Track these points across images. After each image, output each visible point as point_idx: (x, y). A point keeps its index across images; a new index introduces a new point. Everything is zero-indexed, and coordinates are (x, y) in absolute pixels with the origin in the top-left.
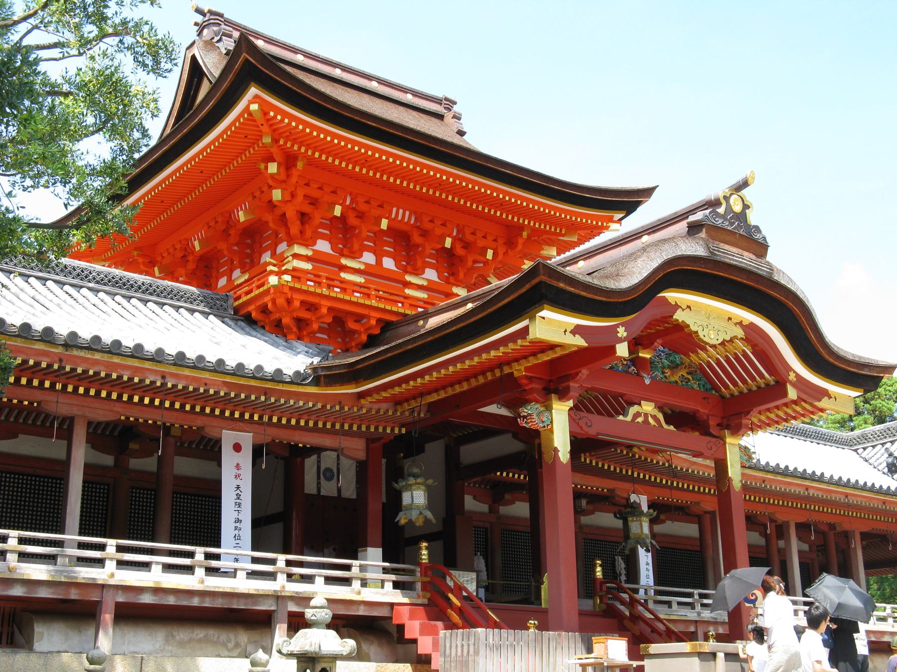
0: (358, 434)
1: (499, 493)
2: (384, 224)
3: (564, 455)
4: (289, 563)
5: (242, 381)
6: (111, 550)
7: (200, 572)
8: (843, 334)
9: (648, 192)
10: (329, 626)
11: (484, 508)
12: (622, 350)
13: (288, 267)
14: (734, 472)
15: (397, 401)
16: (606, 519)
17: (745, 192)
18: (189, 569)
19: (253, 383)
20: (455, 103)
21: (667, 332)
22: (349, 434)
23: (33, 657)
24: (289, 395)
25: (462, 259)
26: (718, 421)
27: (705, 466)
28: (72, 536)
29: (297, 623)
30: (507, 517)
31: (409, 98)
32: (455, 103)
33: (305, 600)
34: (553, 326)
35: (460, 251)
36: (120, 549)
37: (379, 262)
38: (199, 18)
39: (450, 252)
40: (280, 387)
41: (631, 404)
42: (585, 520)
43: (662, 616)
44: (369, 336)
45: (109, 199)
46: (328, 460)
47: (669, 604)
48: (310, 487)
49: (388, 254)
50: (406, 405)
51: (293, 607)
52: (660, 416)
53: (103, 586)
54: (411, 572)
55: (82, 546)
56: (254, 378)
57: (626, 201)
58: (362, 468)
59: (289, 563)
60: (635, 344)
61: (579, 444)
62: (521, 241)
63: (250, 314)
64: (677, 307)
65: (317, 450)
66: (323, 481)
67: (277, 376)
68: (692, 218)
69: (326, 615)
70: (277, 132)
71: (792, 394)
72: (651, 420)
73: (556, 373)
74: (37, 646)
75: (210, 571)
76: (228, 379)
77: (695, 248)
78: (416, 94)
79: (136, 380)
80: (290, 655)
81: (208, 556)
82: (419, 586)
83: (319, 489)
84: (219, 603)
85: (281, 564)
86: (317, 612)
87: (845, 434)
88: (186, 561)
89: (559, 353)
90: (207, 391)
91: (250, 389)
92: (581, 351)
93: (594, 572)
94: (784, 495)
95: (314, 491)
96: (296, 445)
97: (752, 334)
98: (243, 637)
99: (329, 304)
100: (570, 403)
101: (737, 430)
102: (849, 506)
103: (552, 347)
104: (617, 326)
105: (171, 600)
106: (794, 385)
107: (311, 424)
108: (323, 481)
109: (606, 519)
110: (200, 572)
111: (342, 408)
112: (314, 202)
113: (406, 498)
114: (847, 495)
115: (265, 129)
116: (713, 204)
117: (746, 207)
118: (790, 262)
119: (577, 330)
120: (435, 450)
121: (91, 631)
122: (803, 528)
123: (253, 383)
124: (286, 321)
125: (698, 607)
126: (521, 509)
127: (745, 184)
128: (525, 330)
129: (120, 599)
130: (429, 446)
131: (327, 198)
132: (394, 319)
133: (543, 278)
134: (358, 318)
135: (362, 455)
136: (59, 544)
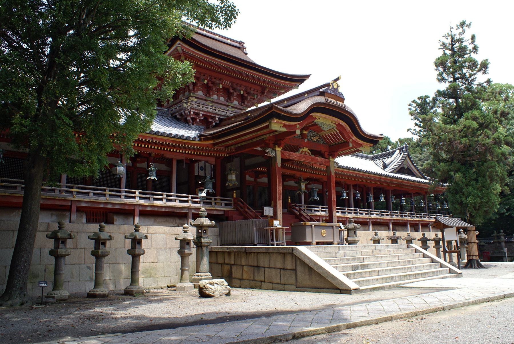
0: (213, 156)
1: (257, 175)
2: (221, 87)
3: (279, 165)
4: (192, 198)
5: (177, 140)
6: (165, 196)
7: (165, 201)
8: (368, 127)
9: (308, 76)
10: (206, 217)
11: (252, 179)
12: (298, 132)
13: (192, 105)
14: (332, 169)
15: (226, 147)
16: (292, 183)
17: (338, 82)
19: (181, 140)
21: (313, 125)
22: (211, 156)
23: (115, 226)
24: (192, 144)
25: (246, 98)
26: (328, 153)
27: (324, 168)
28: (123, 189)
29: (196, 216)
30: (260, 183)
33: (199, 209)
34: (277, 126)
35: (246, 95)
37: (218, 99)
39: (243, 95)
40: (189, 142)
41: (301, 148)
42: (285, 183)
43: (309, 214)
44: (216, 123)
45: (157, 99)
46: (202, 164)
47: (311, 210)
48: (196, 174)
50: (230, 148)
51: (193, 211)
52: (310, 152)
54: (230, 201)
55: (126, 192)
56: (181, 139)
57: (300, 79)
58: (214, 169)
60: (301, 131)
61: (283, 160)
62: (266, 92)
63: (176, 116)
64: (316, 118)
65: (198, 161)
66: (200, 171)
67: (188, 138)
68: (321, 90)
69: (206, 213)
71: (351, 145)
73: (278, 139)
74: (115, 223)
75: (168, 200)
76: (173, 139)
77: (321, 99)
78: (231, 40)
79: (144, 140)
80: (195, 226)
81: (167, 195)
82: (233, 205)
83: (198, 174)
84: (171, 210)
87: (371, 156)
88: (104, 192)
89: (276, 133)
90: (166, 143)
91: (180, 142)
92: (285, 133)
93: (288, 200)
94: (349, 176)
95: (197, 174)
96: (192, 160)
97: (339, 125)
98: (178, 221)
100: (282, 148)
101: (334, 157)
102: (369, 180)
103: (276, 131)
104: (297, 124)
105: (156, 209)
106: (351, 142)
107: (198, 153)
108: (200, 171)
109: (292, 183)
110: (165, 201)
111: (209, 148)
113: (229, 177)
114: (369, 176)
115: (182, 55)
116: (327, 85)
117: (338, 87)
118: (352, 104)
119: (284, 126)
120: (237, 160)
121: (132, 219)
122: (355, 187)
123: (181, 140)
124: (189, 118)
125: (320, 211)
126: (265, 180)
127: (338, 79)
128: (267, 127)
129: (141, 209)
130: (235, 160)
131: (202, 77)
132: (223, 118)
133: (274, 110)
134: (213, 118)
135: (214, 163)
136: (120, 191)
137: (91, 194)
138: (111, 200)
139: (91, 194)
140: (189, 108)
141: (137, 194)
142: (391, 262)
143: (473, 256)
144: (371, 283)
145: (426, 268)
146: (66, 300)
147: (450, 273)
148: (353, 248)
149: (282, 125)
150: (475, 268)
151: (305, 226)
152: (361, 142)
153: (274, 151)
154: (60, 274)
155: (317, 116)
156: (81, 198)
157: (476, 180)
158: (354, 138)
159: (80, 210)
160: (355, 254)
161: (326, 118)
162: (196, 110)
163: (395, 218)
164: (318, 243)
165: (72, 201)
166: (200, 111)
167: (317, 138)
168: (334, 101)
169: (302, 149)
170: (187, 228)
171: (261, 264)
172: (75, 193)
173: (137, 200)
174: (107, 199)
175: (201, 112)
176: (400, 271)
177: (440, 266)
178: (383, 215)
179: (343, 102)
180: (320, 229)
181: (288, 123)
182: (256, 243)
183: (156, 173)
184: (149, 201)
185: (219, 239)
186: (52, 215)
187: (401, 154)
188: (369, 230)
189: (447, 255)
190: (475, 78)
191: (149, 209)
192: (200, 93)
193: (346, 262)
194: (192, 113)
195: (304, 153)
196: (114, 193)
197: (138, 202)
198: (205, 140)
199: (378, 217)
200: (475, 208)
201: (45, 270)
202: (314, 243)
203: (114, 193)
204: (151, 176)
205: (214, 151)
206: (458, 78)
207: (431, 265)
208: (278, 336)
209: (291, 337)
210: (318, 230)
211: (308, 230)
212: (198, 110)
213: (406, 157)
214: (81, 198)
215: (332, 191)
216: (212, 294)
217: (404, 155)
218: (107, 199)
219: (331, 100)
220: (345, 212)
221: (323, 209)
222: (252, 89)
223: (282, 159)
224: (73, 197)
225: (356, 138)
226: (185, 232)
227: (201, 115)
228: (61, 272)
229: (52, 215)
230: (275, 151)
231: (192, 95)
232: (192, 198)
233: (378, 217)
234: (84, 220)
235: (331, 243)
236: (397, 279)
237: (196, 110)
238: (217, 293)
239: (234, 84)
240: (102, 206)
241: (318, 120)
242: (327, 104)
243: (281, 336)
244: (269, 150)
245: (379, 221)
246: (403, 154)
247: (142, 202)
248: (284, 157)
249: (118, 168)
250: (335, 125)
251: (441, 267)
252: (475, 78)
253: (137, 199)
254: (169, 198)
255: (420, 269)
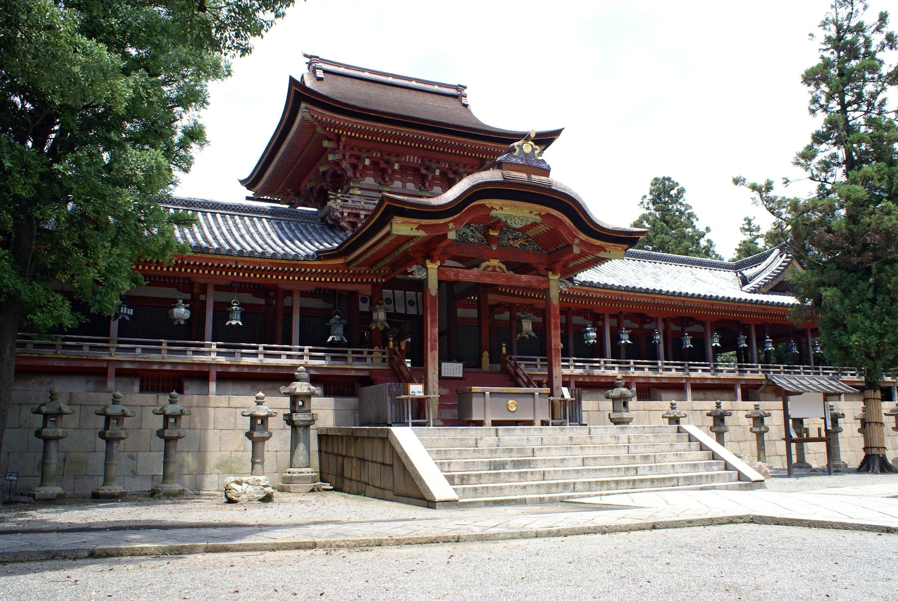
6: (261, 349)
9: (557, 133)
18: (256, 355)
20: (465, 88)
31: (436, 88)
32: (465, 88)
36: (265, 348)
37: (404, 187)
38: (308, 60)
41: (484, 261)
43: (526, 373)
49: (410, 181)
52: (504, 267)
53: (210, 364)
59: (265, 348)
64: (492, 209)
70: (325, 125)
71: (576, 250)
72: (498, 269)
84: (271, 371)
85: (632, 364)
86: (301, 372)
88: (254, 351)
93: (501, 351)
99: (364, 213)
104: (448, 223)
105: (246, 370)
112: (358, 158)
123: (284, 262)
124: (343, 224)
128: (389, 234)
129: (219, 370)
137: (139, 351)
138: (170, 358)
139: (139, 351)
140: (338, 207)
141: (214, 347)
142: (595, 458)
143: (872, 448)
144: (506, 492)
145: (685, 470)
146: (52, 499)
147: (739, 479)
148: (532, 431)
149: (415, 227)
150: (873, 472)
151: (471, 393)
152: (598, 243)
153: (424, 270)
154: (48, 464)
155: (497, 204)
156: (121, 357)
157: (873, 301)
158: (583, 237)
159: (122, 373)
160: (525, 442)
161: (516, 207)
162: (352, 209)
163: (749, 376)
164: (495, 423)
165: (108, 360)
166: (361, 210)
167: (522, 241)
168: (524, 176)
169: (487, 263)
170: (263, 398)
171: (368, 456)
172: (114, 350)
173: (213, 355)
174: (166, 356)
175: (361, 212)
176: (604, 474)
177: (723, 467)
178: (721, 371)
179: (548, 176)
180: (505, 399)
181: (425, 222)
182: (389, 423)
183: (241, 315)
184: (232, 359)
185: (357, 415)
186: (87, 382)
187: (781, 256)
188: (685, 399)
189: (793, 445)
190: (884, 100)
191: (233, 370)
192: (370, 181)
193: (489, 456)
194: (346, 214)
195: (491, 269)
196: (175, 348)
197: (214, 359)
198: (327, 257)
199: (708, 375)
200: (868, 355)
201: (65, 459)
202: (488, 422)
203: (175, 348)
204: (232, 319)
205: (349, 275)
206: (850, 104)
207: (710, 464)
208: (61, 551)
209: (86, 554)
210: (496, 399)
211: (476, 402)
212: (356, 209)
213: (789, 263)
214: (121, 357)
215: (553, 332)
216: (235, 498)
217: (787, 257)
218: (166, 356)
219: (514, 174)
220: (629, 368)
221: (577, 364)
222: (461, 165)
223: (440, 282)
224: (111, 355)
225: (587, 237)
226: (258, 404)
227: (362, 217)
228: (50, 461)
229: (87, 382)
230: (426, 268)
231: (352, 184)
232: (310, 350)
233: (708, 375)
234: (137, 388)
235: (530, 423)
236: (578, 487)
237: (352, 209)
238: (244, 496)
239: (426, 160)
240: (156, 367)
241: (500, 212)
242: (506, 182)
243: (66, 551)
244: (414, 268)
245: (708, 382)
246: (785, 256)
247: (222, 360)
248: (444, 278)
249: (175, 310)
250: (538, 218)
251: (726, 469)
252: (884, 100)
253: (214, 356)
254: (269, 352)
255: (663, 471)
